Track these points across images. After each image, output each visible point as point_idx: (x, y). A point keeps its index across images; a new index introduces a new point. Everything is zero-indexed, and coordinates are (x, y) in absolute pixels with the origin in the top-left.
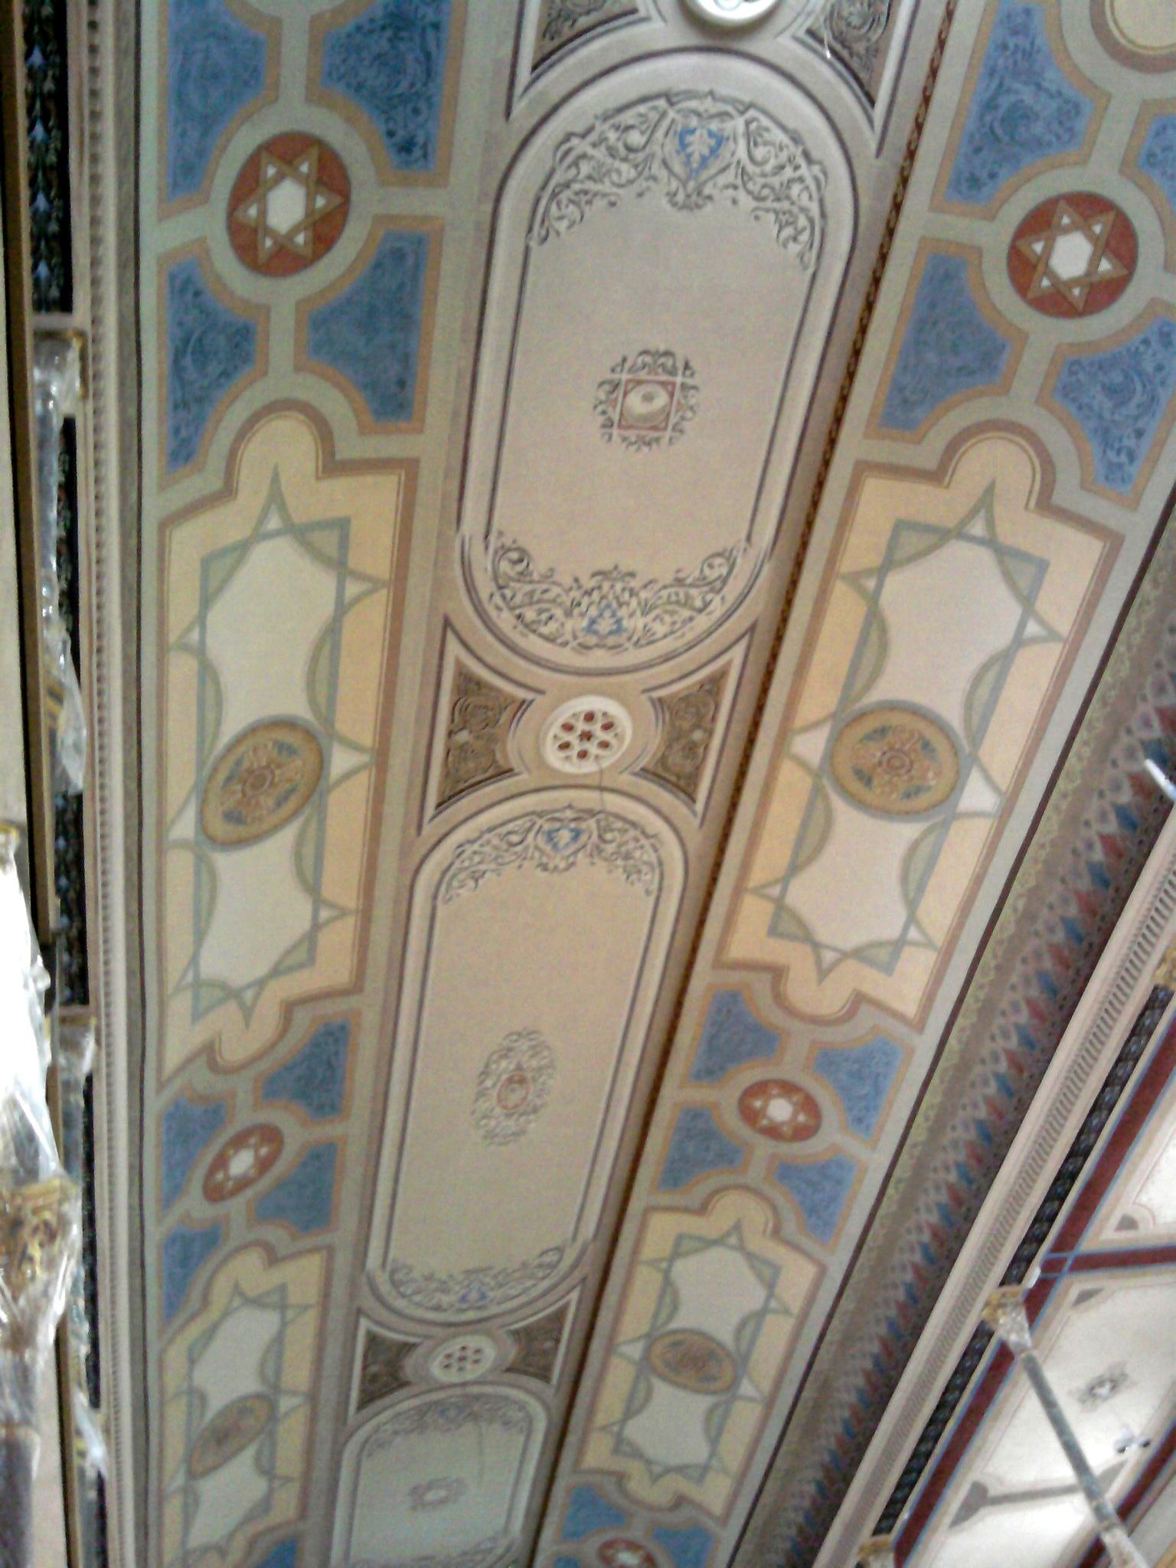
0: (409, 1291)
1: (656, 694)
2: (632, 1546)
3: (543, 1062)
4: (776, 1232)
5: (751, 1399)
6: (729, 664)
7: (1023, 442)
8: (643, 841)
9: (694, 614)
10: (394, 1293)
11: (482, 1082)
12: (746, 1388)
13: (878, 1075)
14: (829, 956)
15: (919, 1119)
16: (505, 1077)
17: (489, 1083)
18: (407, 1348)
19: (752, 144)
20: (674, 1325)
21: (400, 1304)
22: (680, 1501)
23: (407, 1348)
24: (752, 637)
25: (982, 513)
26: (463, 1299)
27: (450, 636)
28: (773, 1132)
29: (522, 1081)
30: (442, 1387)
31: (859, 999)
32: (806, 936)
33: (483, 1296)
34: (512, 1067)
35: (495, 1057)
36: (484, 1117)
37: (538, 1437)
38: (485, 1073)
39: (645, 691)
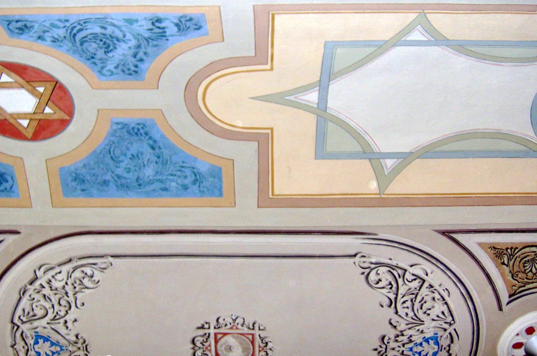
1: (504, 298)
6: (480, 244)
8: (43, 281)
9: (426, 285)
19: (35, 318)
39: (501, 309)
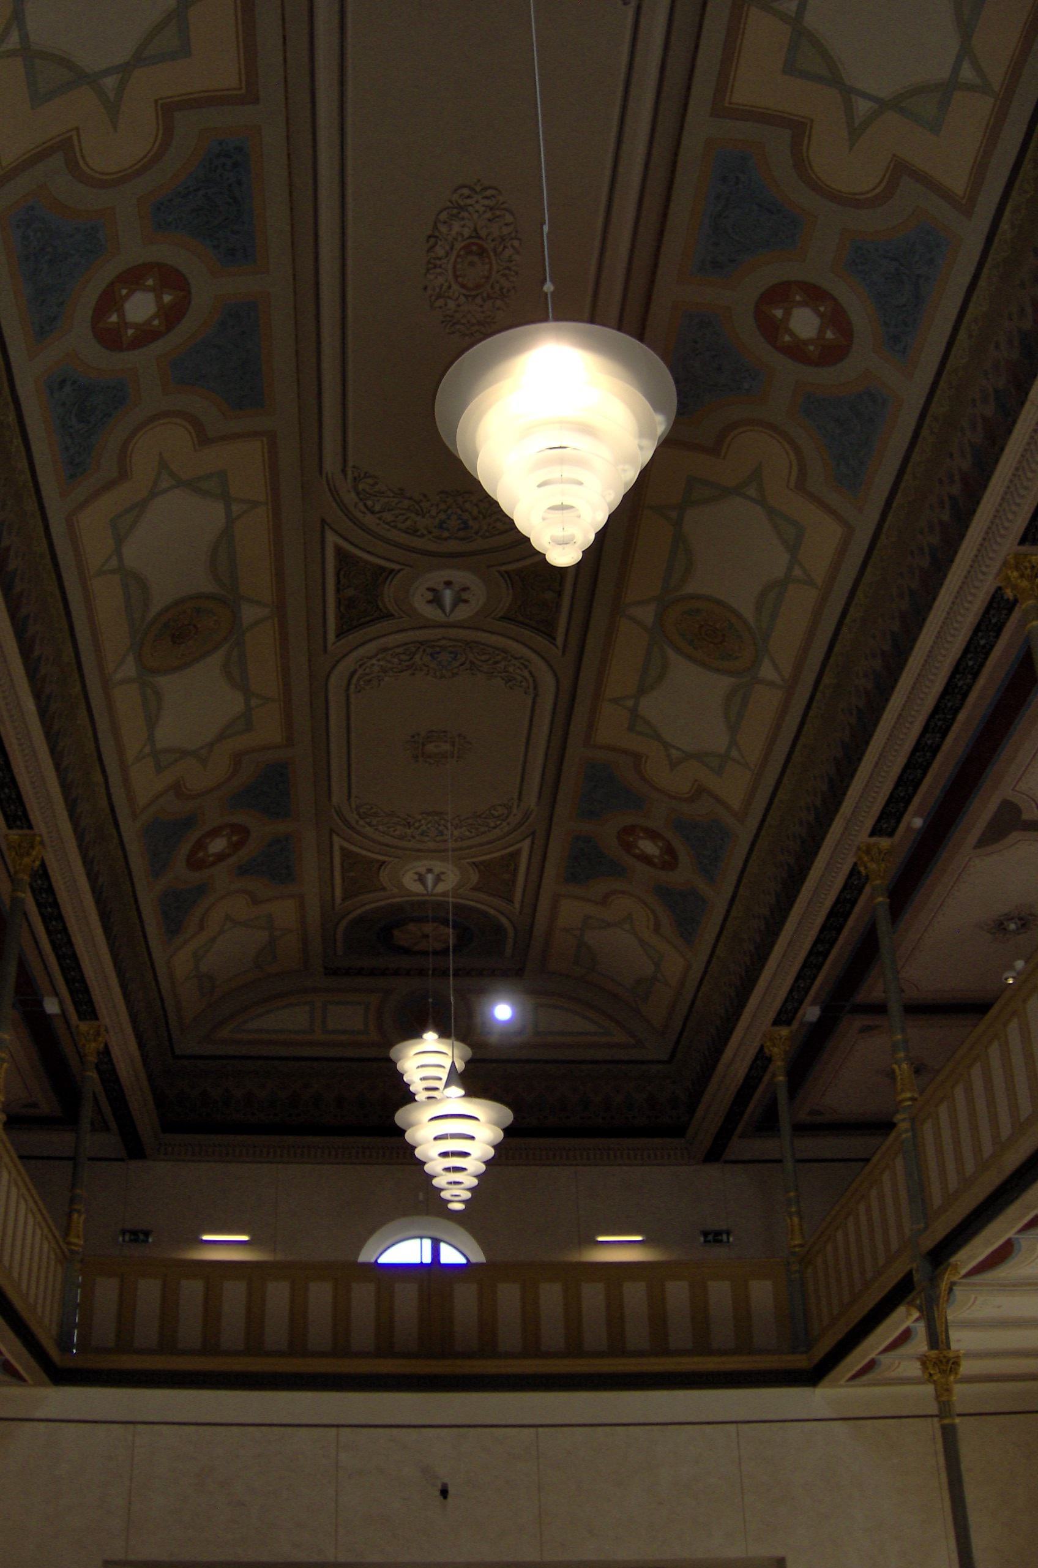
0: (377, 508)
2: (653, 835)
3: (506, 231)
4: (801, 486)
5: (772, 684)
7: (787, 446)
10: (361, 506)
11: (431, 249)
12: (766, 671)
13: (919, 276)
14: (863, 107)
15: (962, 335)
16: (458, 246)
17: (440, 251)
18: (382, 575)
20: (689, 589)
21: (369, 520)
22: (700, 791)
23: (382, 575)
24: (328, 525)
25: (857, 122)
26: (441, 526)
27: (326, 527)
28: (796, 351)
29: (482, 252)
30: (427, 625)
31: (900, 169)
32: (834, 79)
33: (466, 526)
34: (466, 232)
35: (443, 216)
36: (439, 297)
37: (547, 701)
38: (433, 237)
